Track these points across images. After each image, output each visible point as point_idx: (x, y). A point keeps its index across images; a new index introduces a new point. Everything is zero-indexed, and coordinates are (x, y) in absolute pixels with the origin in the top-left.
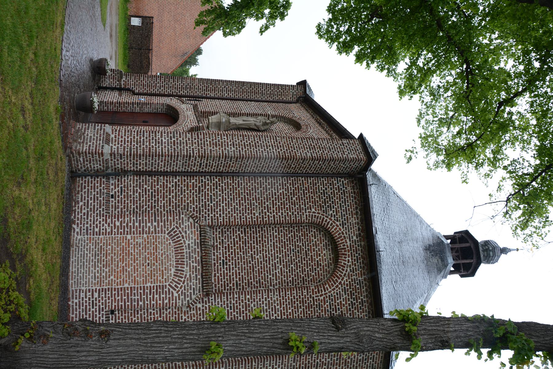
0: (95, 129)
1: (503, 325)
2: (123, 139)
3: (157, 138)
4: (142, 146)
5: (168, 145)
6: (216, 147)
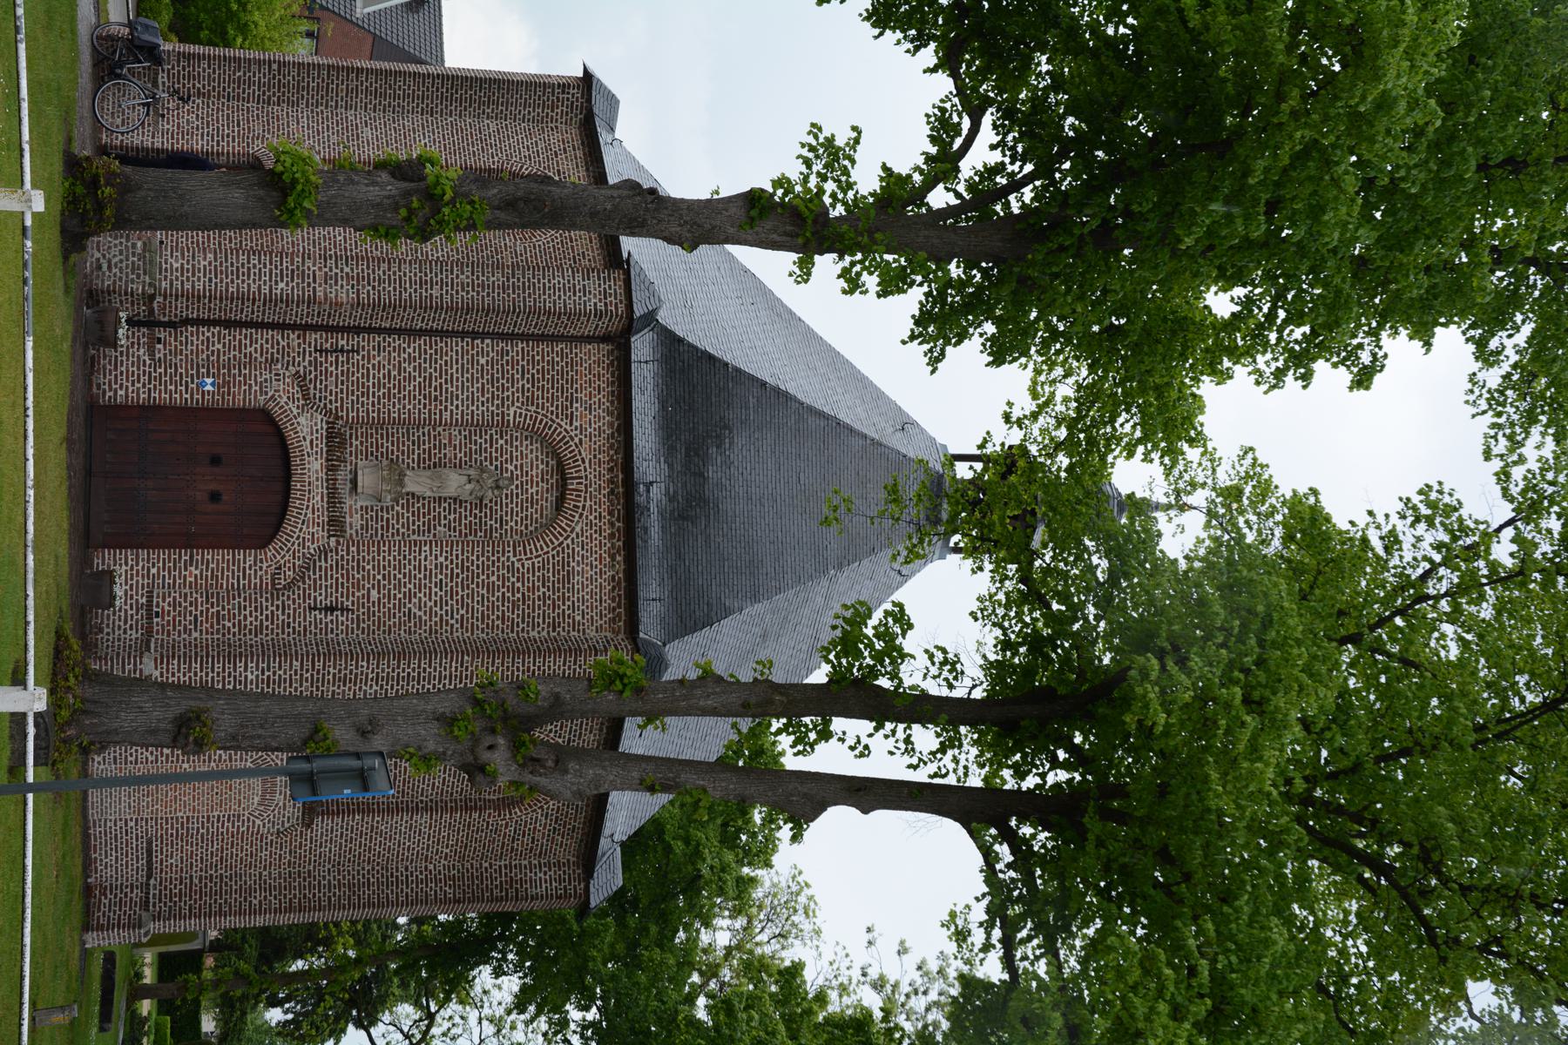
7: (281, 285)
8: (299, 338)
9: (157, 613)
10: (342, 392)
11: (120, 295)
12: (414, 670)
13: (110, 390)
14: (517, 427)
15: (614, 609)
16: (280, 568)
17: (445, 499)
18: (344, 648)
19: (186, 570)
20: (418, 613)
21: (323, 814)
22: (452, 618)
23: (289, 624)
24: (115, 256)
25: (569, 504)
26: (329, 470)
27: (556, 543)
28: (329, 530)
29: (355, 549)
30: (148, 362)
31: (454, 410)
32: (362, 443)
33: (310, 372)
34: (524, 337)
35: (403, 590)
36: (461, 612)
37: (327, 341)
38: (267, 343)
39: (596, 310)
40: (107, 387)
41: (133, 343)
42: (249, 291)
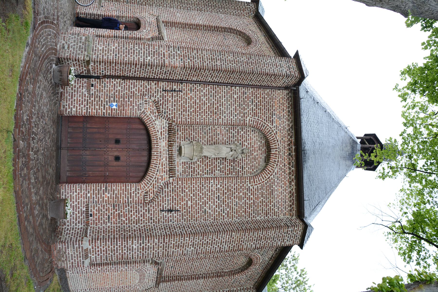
0: (74, 248)
1: (392, 7)
2: (99, 249)
3: (129, 246)
4: (116, 254)
5: (138, 251)
6: (178, 248)
7: (149, 58)
8: (155, 84)
9: (91, 215)
10: (174, 110)
11: (73, 61)
12: (210, 240)
13: (69, 108)
14: (250, 126)
15: (291, 206)
16: (147, 193)
17: (219, 158)
18: (178, 231)
19: (104, 194)
20: (209, 211)
21: (163, 282)
22: (224, 213)
23: (151, 218)
24: (72, 43)
25: (272, 160)
26: (169, 146)
27: (267, 177)
28: (169, 174)
29: (180, 182)
30: (87, 95)
31: (224, 118)
32: (182, 133)
33: (161, 100)
34: (253, 86)
35: (202, 201)
36: (228, 210)
37: (168, 86)
38: (141, 86)
39: (287, 74)
40: (67, 107)
41: (80, 86)
42: (134, 60)
